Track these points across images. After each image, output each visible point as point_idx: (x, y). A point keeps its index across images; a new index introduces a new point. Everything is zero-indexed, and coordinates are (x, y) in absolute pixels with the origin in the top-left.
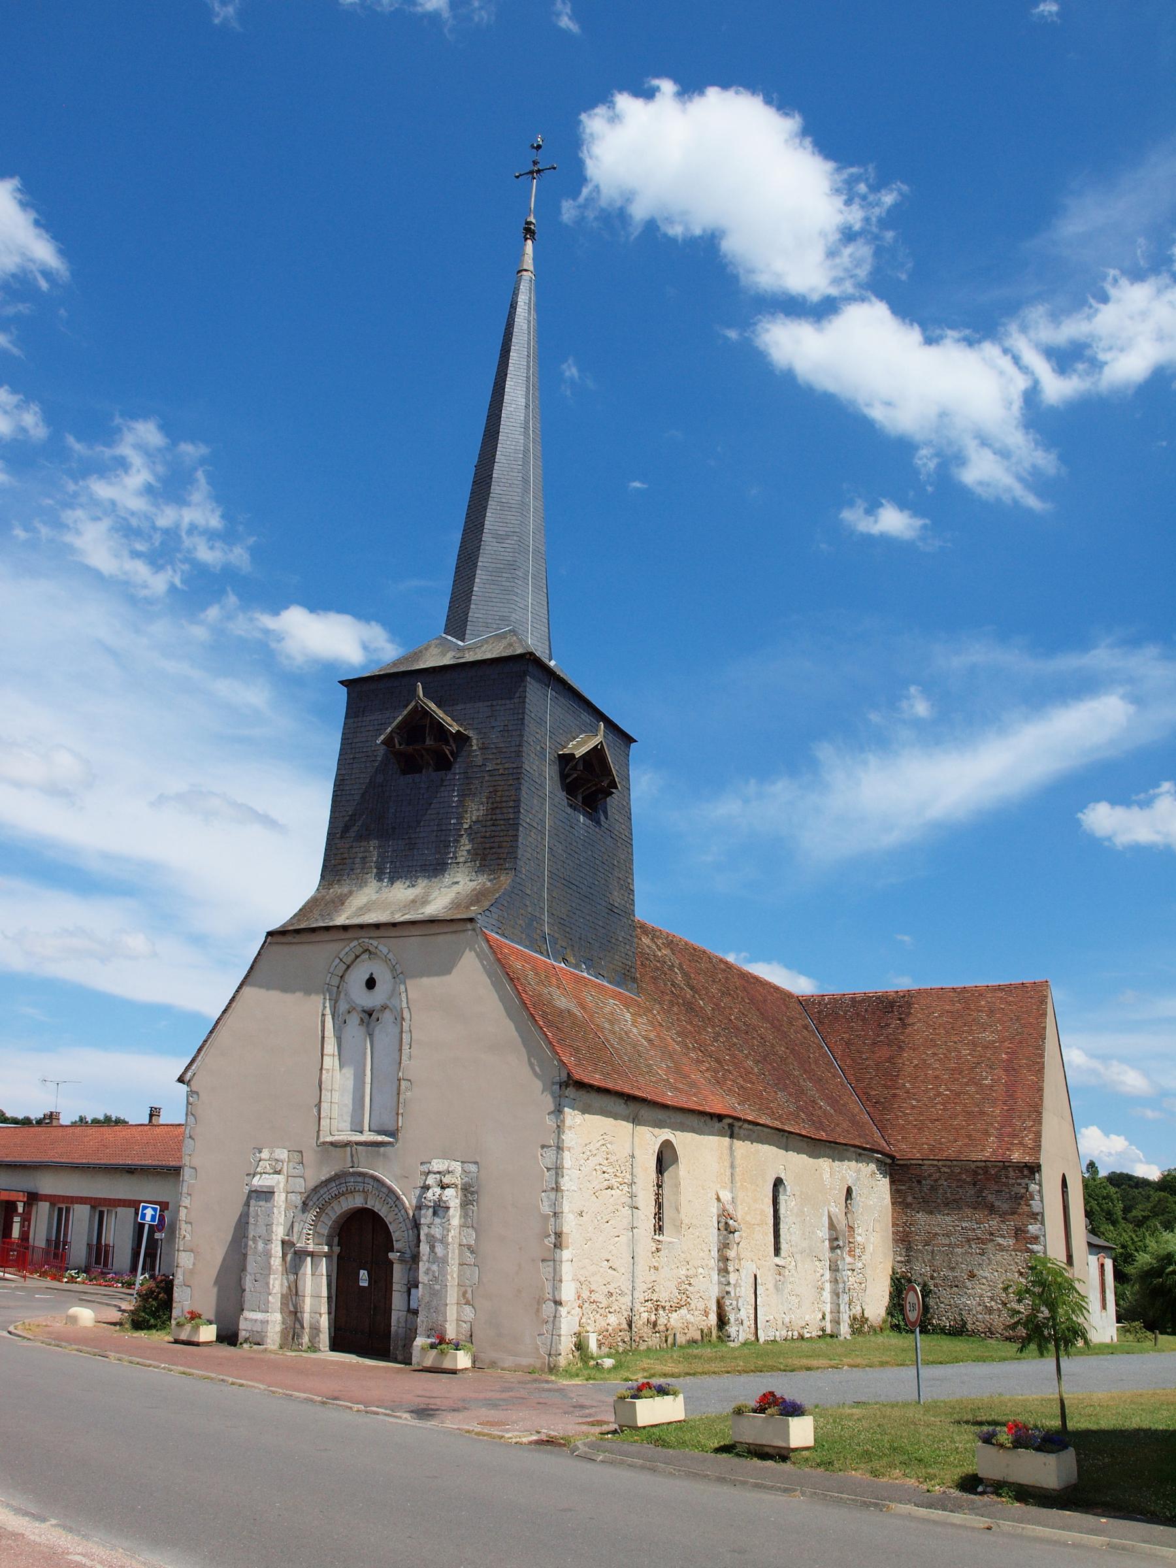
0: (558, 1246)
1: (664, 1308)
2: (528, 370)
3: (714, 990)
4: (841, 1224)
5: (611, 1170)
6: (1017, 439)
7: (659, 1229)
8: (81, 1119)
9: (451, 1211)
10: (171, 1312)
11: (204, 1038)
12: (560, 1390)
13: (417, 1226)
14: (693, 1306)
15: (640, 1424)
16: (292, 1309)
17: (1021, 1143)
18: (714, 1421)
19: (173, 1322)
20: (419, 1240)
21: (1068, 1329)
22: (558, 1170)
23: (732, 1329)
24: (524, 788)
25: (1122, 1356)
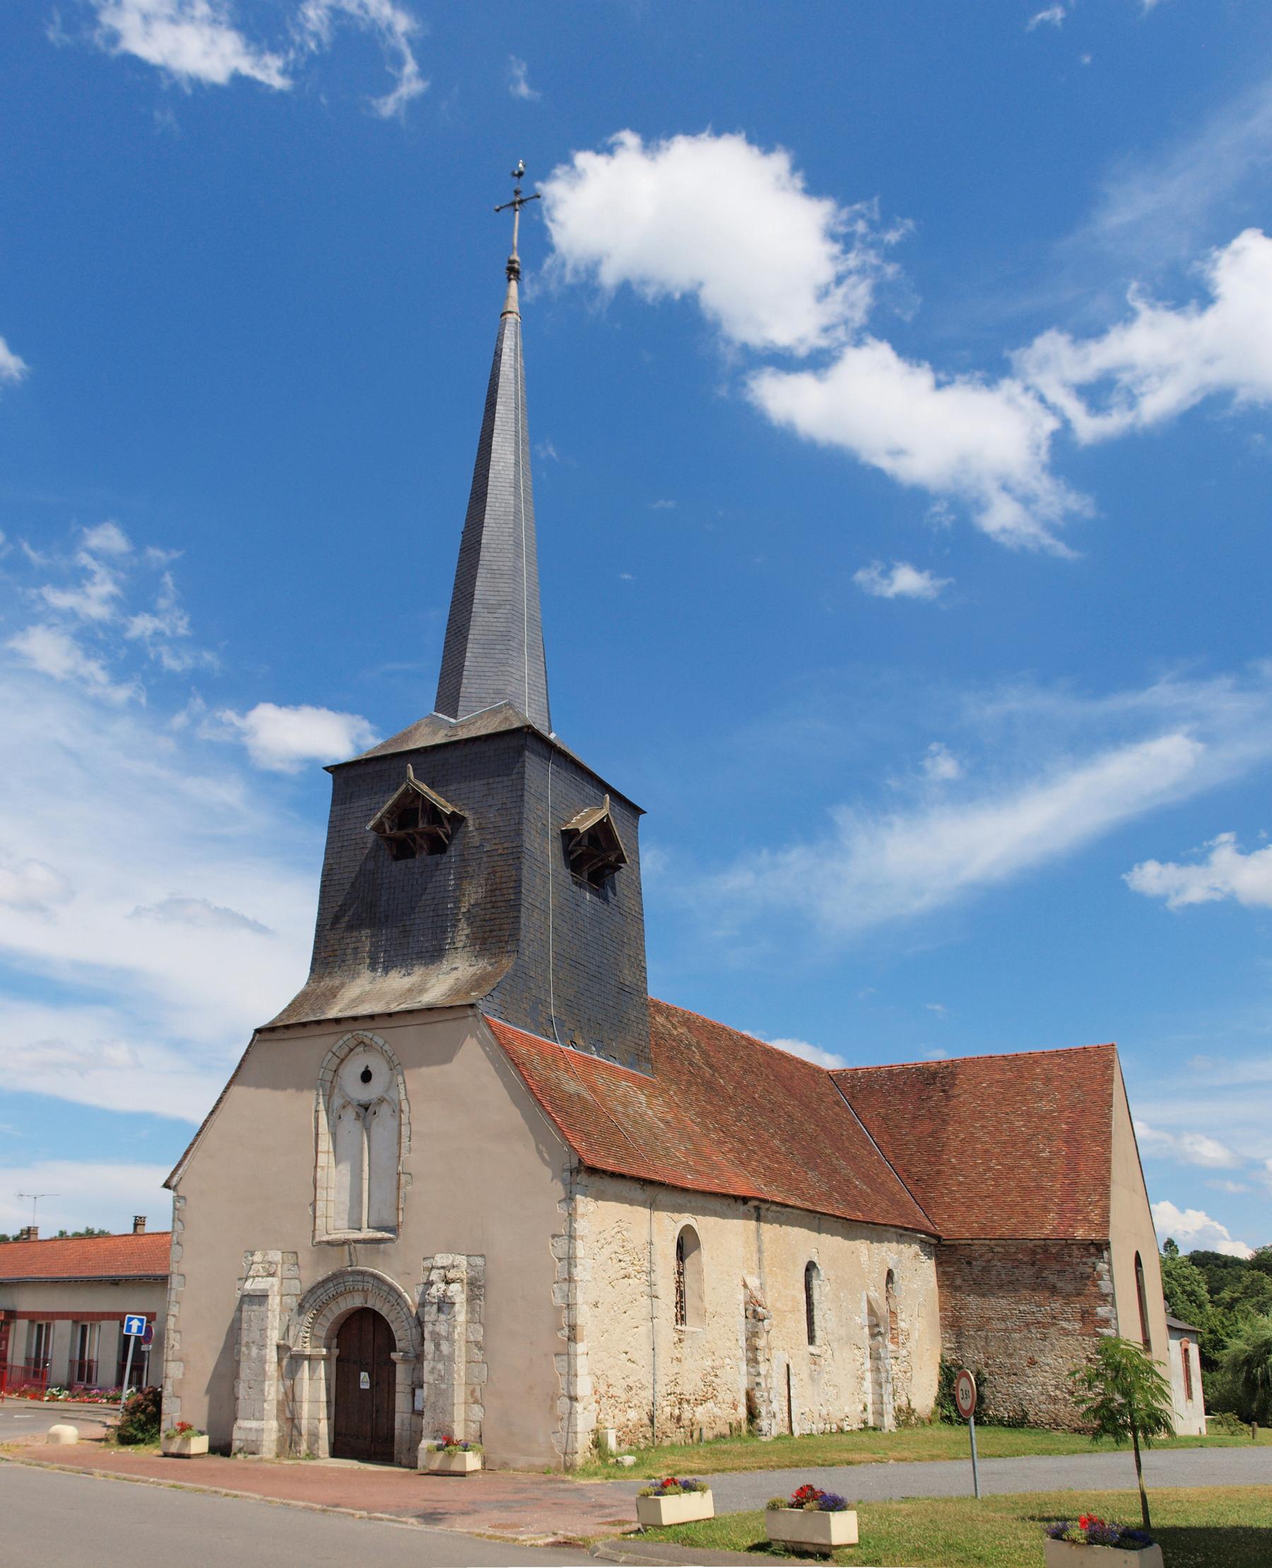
0: (572, 1339)
1: (688, 1401)
2: (517, 424)
3: (735, 1067)
4: (882, 1308)
5: (627, 1258)
6: (1043, 486)
7: (681, 1318)
8: (62, 1233)
9: (457, 1307)
10: (160, 1424)
11: (191, 1141)
12: (577, 1490)
13: (420, 1323)
14: (720, 1399)
15: (665, 1523)
16: (289, 1415)
17: (1085, 1219)
18: (746, 1519)
19: (163, 1435)
20: (423, 1339)
21: (1149, 1416)
22: (570, 1260)
23: (763, 1423)
24: (525, 867)
25: (1213, 1449)
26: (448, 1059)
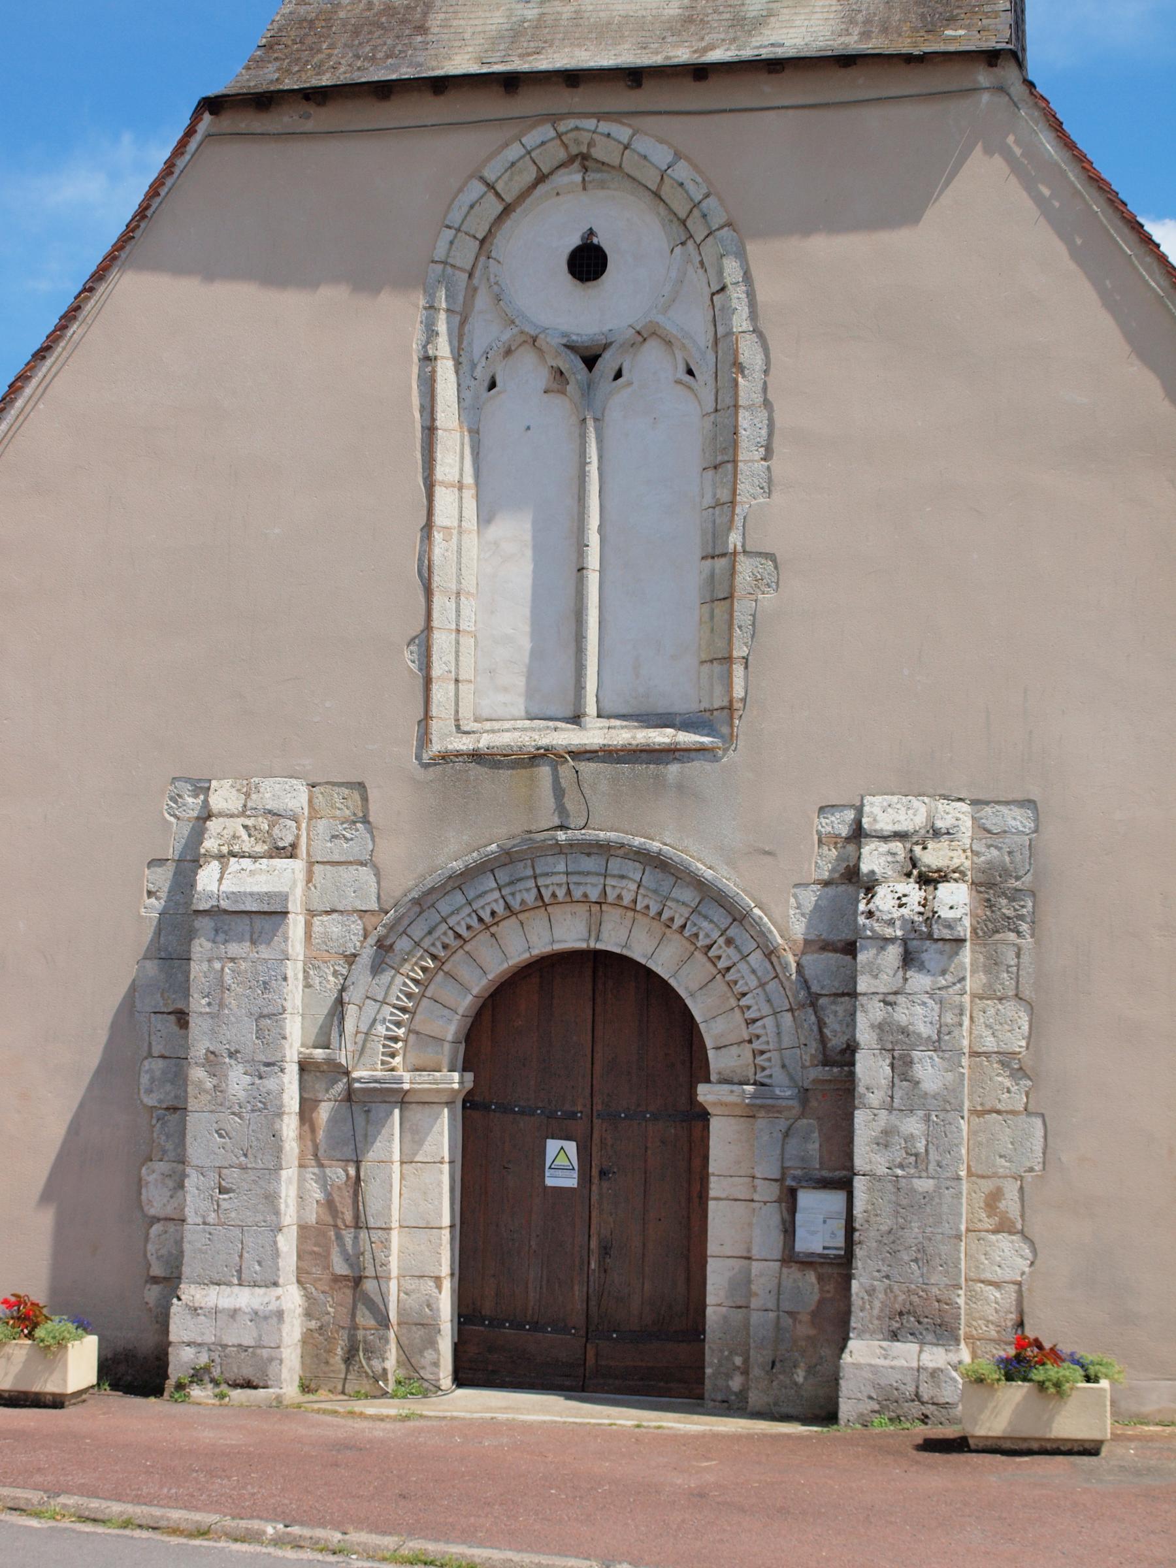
16: (340, 1267)
26: (903, 209)
